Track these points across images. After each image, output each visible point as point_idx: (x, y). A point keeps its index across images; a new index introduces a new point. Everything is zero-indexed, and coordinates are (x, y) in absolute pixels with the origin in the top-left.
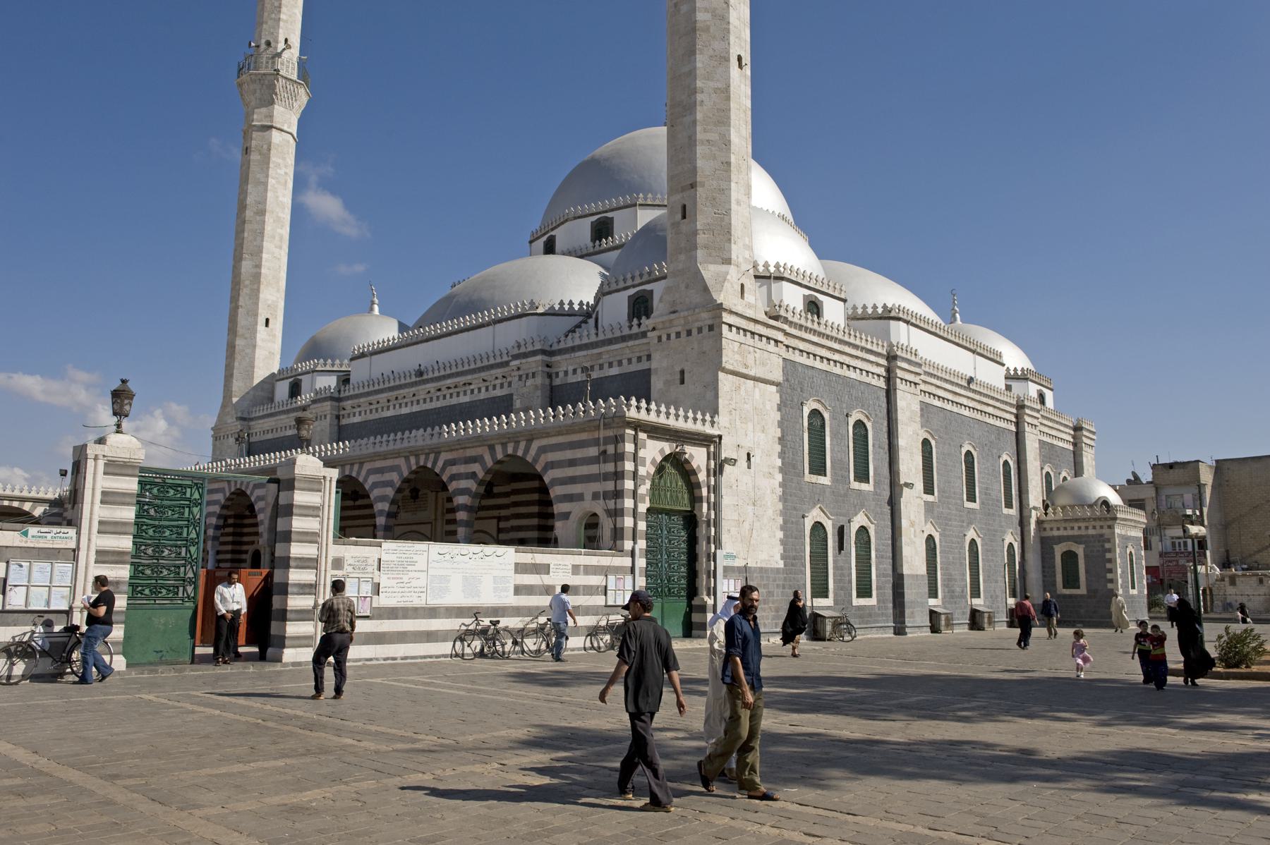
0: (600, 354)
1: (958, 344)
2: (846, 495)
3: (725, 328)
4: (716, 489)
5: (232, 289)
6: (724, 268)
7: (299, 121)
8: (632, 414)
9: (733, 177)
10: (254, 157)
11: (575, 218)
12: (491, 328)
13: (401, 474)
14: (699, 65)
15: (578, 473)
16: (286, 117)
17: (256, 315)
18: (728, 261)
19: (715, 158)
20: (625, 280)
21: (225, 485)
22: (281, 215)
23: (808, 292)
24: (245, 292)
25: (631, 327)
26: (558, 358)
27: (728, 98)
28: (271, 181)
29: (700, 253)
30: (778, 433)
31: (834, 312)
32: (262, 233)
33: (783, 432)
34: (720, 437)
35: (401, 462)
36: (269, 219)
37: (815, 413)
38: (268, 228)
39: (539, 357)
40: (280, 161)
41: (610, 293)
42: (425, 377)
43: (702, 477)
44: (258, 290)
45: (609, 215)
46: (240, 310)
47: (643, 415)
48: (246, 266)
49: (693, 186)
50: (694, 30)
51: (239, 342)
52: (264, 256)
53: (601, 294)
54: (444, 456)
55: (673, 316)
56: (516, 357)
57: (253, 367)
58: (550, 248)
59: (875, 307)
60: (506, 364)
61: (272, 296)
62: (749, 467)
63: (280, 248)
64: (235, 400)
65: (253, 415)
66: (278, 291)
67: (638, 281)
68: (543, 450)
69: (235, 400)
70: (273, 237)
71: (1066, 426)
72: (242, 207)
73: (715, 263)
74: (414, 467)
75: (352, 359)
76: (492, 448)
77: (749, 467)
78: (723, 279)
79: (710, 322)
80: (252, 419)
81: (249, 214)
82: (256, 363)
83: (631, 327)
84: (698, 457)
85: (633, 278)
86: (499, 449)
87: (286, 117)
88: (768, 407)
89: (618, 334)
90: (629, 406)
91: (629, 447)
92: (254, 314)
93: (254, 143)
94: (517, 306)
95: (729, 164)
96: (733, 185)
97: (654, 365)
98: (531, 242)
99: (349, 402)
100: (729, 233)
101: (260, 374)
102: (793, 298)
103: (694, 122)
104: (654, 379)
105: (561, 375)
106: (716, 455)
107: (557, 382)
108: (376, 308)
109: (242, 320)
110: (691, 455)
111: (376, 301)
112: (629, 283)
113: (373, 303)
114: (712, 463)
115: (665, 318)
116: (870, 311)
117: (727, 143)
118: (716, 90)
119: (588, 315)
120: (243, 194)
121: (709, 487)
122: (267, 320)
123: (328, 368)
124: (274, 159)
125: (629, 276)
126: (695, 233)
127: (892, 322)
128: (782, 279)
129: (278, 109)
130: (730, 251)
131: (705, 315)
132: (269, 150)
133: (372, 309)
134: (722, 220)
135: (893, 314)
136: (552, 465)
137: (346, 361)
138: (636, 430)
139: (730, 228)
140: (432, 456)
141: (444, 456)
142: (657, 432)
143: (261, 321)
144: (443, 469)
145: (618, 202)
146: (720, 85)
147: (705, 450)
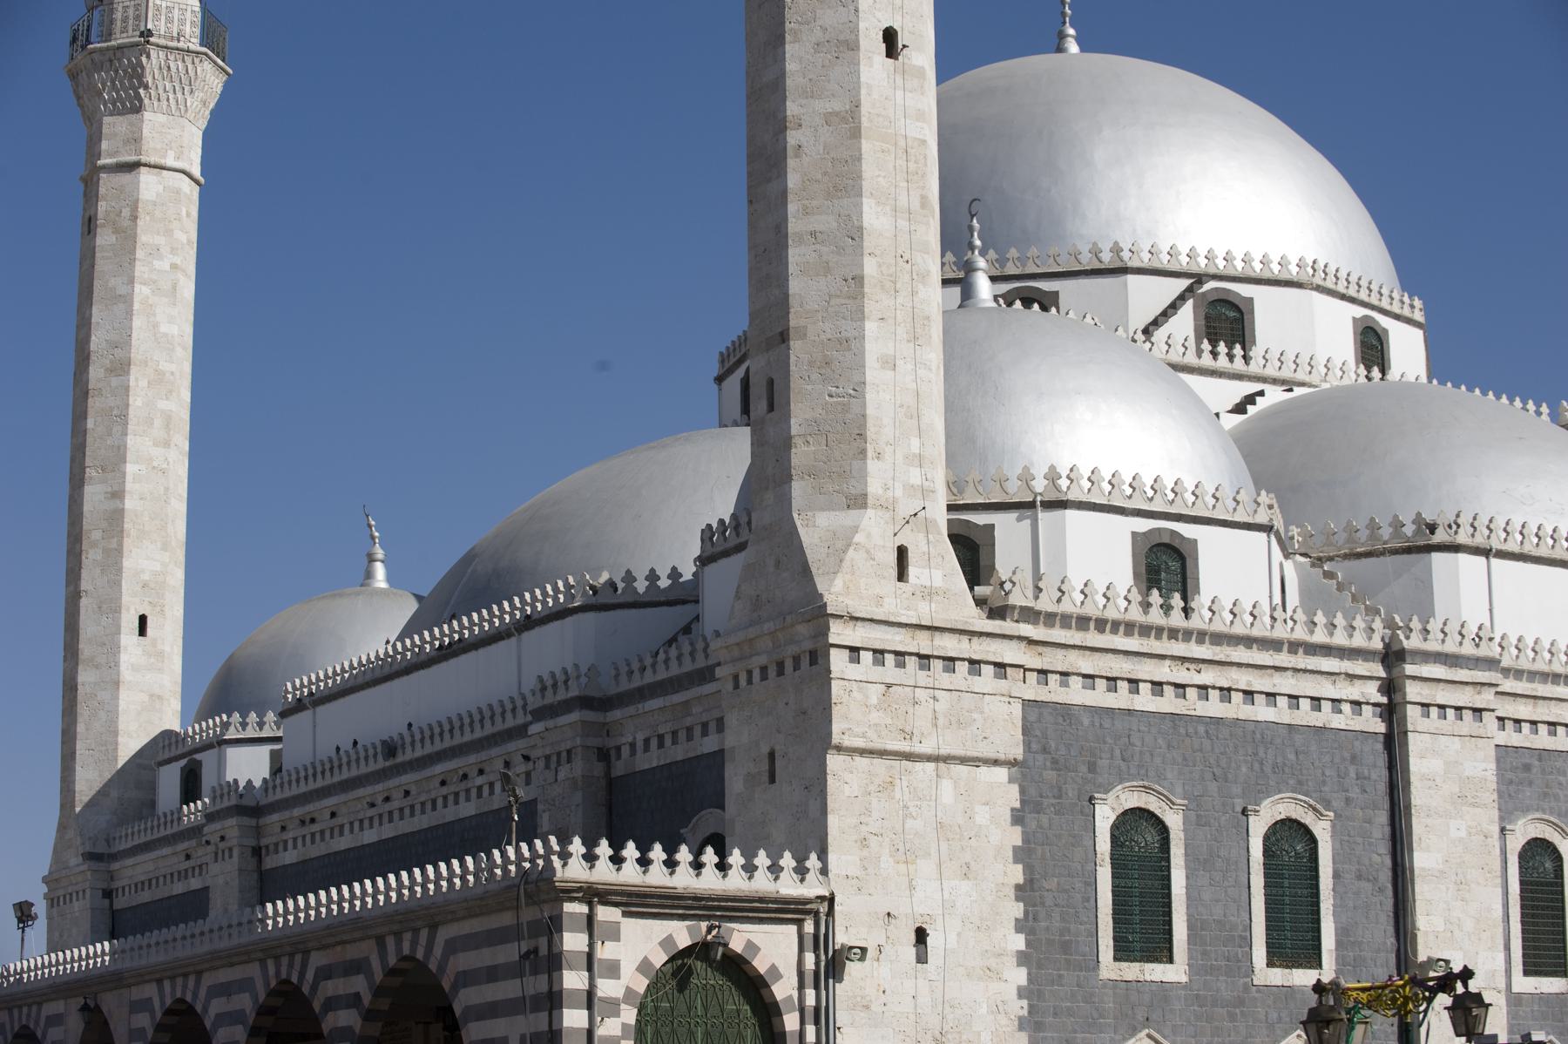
0: (686, 703)
2: (1241, 1002)
4: (821, 1016)
5: (69, 552)
6: (845, 518)
7: (206, 135)
8: (574, 870)
9: (870, 306)
10: (104, 238)
13: (255, 998)
14: (790, 66)
15: (500, 996)
16: (172, 131)
17: (117, 610)
18: (859, 501)
19: (827, 269)
21: (367, 949)
22: (165, 366)
23: (1144, 525)
24: (91, 557)
26: (617, 714)
27: (856, 133)
28: (141, 291)
29: (798, 489)
30: (1017, 874)
31: (1239, 573)
32: (123, 417)
33: (1029, 870)
34: (831, 900)
35: (253, 970)
36: (138, 380)
37: (1134, 821)
38: (137, 402)
39: (574, 716)
40: (160, 240)
42: (400, 759)
43: (784, 990)
44: (119, 551)
46: (84, 602)
47: (604, 872)
48: (94, 496)
49: (784, 337)
51: (85, 677)
52: (131, 468)
54: (317, 960)
56: (540, 714)
57: (116, 733)
60: (521, 731)
61: (151, 556)
62: (922, 959)
63: (167, 444)
64: (78, 809)
65: (114, 850)
66: (165, 547)
68: (452, 947)
69: (78, 809)
70: (150, 422)
71: (492, 1010)
72: (83, 358)
73: (830, 507)
74: (392, 960)
75: (283, 715)
76: (381, 941)
77: (922, 959)
78: (842, 543)
79: (808, 645)
80: (114, 857)
81: (95, 372)
82: (122, 725)
84: (774, 949)
86: (390, 942)
87: (172, 131)
88: (982, 816)
90: (565, 856)
91: (574, 941)
92: (112, 607)
93: (102, 207)
95: (859, 280)
96: (870, 327)
97: (730, 740)
98: (719, 380)
99: (275, 817)
100: (862, 435)
101: (130, 743)
104: (729, 771)
105: (625, 751)
106: (820, 942)
107: (619, 769)
108: (380, 571)
109: (89, 626)
110: (750, 945)
111: (379, 553)
113: (371, 559)
114: (810, 958)
116: (1386, 532)
117: (855, 234)
118: (829, 118)
120: (84, 326)
121: (802, 1010)
122: (143, 620)
123: (251, 733)
124: (146, 236)
127: (1436, 557)
128: (1062, 504)
129: (153, 120)
130: (863, 476)
131: (803, 629)
132: (134, 218)
133: (369, 574)
134: (846, 408)
135: (1440, 537)
136: (467, 978)
137: (271, 716)
138: (590, 904)
139: (863, 425)
140: (298, 958)
141: (317, 960)
142: (640, 903)
143: (130, 622)
144: (314, 987)
146: (836, 105)
147: (793, 928)
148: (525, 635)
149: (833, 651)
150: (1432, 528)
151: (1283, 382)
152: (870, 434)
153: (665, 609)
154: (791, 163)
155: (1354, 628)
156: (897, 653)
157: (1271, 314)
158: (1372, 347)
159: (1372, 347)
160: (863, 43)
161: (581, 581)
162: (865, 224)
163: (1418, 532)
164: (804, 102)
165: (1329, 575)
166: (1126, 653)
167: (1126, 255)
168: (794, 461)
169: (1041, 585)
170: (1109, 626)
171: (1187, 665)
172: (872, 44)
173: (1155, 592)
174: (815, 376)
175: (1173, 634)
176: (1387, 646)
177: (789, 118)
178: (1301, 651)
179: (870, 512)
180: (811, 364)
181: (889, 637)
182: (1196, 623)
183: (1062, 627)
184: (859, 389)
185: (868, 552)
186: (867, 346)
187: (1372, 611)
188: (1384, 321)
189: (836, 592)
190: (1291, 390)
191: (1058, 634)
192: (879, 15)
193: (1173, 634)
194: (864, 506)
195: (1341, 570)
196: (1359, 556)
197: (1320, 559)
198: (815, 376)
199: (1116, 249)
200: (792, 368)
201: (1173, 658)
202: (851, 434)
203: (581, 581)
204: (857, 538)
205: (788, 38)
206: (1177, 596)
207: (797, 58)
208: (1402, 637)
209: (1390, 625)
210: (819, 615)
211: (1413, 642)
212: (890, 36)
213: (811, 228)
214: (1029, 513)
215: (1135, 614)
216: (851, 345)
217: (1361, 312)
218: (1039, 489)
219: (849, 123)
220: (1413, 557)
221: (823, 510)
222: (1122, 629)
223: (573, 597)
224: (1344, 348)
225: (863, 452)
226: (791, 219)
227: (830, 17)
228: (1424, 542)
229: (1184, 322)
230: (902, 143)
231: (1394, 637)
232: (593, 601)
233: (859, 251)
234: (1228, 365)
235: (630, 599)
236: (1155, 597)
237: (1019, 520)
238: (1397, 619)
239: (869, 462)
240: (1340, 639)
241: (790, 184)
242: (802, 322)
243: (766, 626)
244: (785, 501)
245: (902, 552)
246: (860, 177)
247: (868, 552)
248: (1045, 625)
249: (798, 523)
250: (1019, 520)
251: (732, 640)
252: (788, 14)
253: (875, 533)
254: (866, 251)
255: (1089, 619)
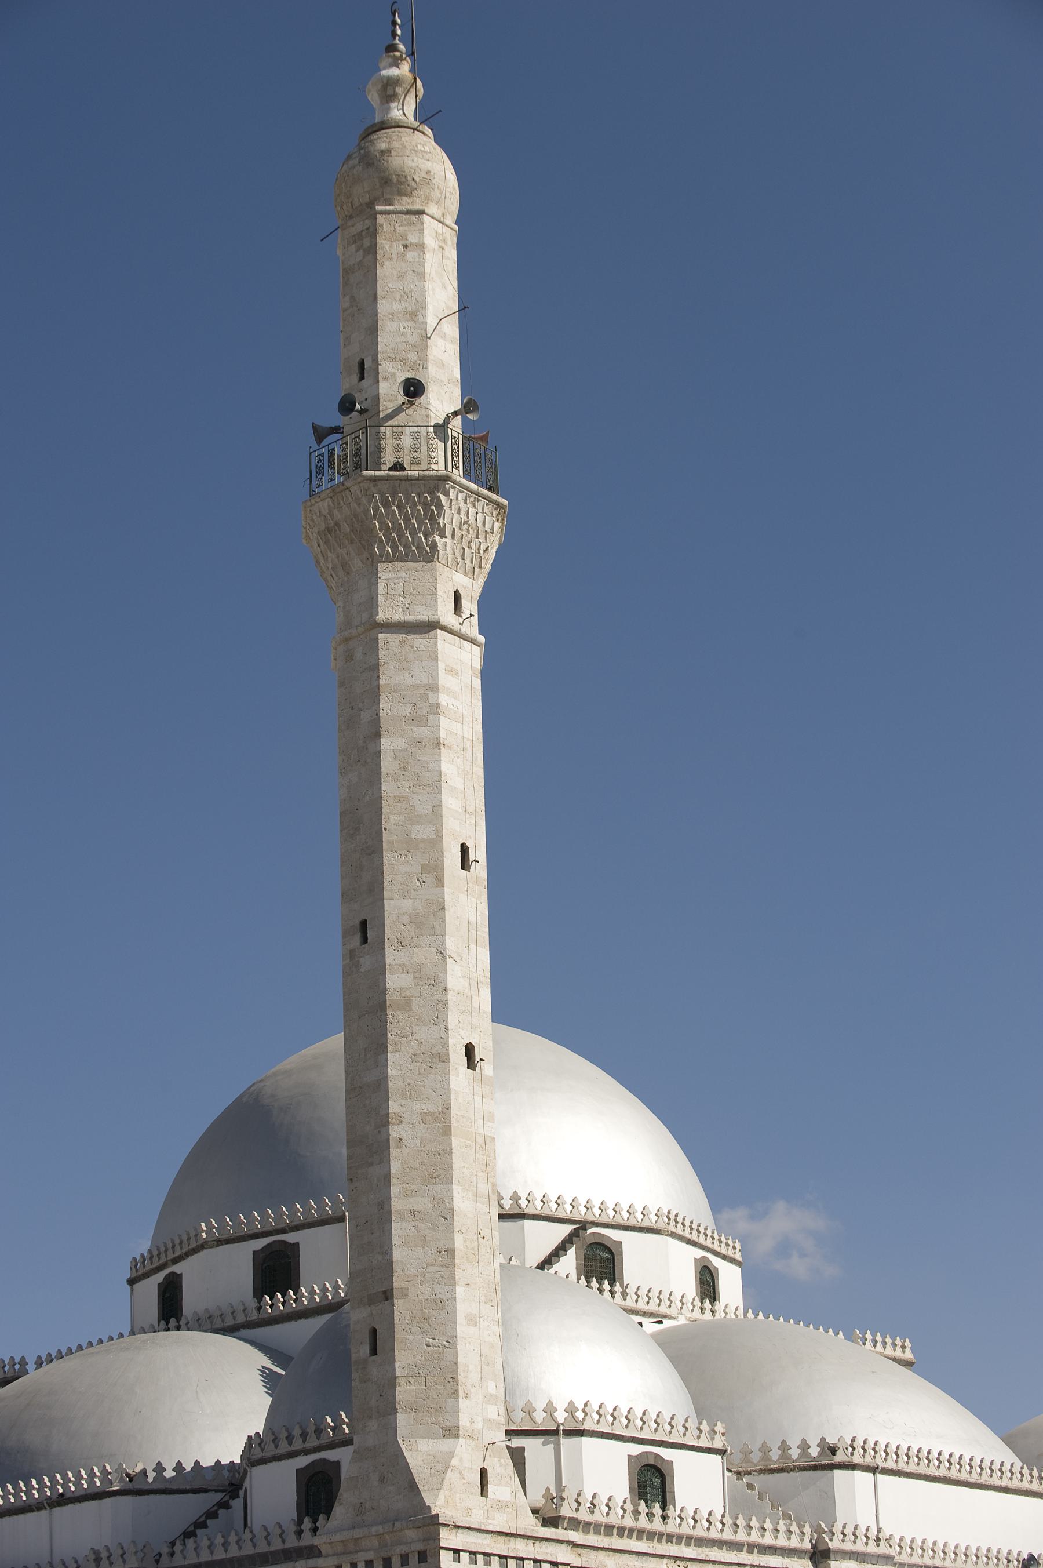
1: (1006, 1490)
3: (445, 1557)
6: (445, 1445)
9: (459, 1274)
11: (220, 1242)
12: (44, 1513)
14: (392, 1071)
18: (453, 1432)
19: (424, 1243)
20: (290, 1439)
23: (637, 1449)
25: (299, 1533)
27: (447, 1131)
29: (402, 1420)
31: (699, 1485)
41: (263, 1461)
45: (290, 1238)
49: (388, 1295)
50: (382, 1006)
53: (257, 1452)
55: (358, 1533)
58: (170, 1310)
59: (804, 1446)
67: (312, 1442)
73: (428, 1436)
78: (442, 1465)
79: (419, 1546)
83: (299, 1533)
85: (304, 1435)
89: (277, 1545)
94: (92, 1475)
95: (451, 1252)
96: (460, 1290)
98: (132, 1282)
100: (454, 1379)
102: (602, 1474)
103: (387, 1178)
112: (298, 1444)
115: (346, 1535)
116: (795, 1453)
117: (448, 1215)
118: (424, 1117)
119: (226, 1485)
125: (297, 1432)
126: (392, 1382)
127: (837, 1473)
128: (580, 1433)
130: (456, 1412)
131: (411, 1534)
134: (441, 1356)
139: (456, 1371)
145: (307, 1209)
146: (430, 1107)
148: (57, 1510)
149: (442, 1552)
150: (833, 1451)
151: (651, 1315)
152: (461, 1378)
153: (190, 1495)
154: (393, 1152)
155: (751, 1528)
156: (485, 1554)
157: (637, 1255)
158: (707, 1284)
159: (707, 1284)
160: (452, 1057)
161: (119, 1469)
162: (455, 1207)
163: (820, 1454)
164: (403, 1102)
165: (750, 1486)
166: (638, 1553)
167: (523, 1203)
168: (399, 1397)
169: (564, 1495)
170: (615, 1531)
171: (678, 1563)
172: (458, 1057)
173: (642, 1502)
174: (415, 1329)
175: (651, 1536)
176: (814, 1546)
177: (391, 1115)
178: (756, 1551)
179: (461, 1441)
180: (412, 1319)
181: (479, 1541)
182: (672, 1527)
183: (595, 1533)
184: (452, 1341)
185: (461, 1473)
186: (458, 1306)
187: (787, 1517)
188: (716, 1261)
189: (442, 1503)
190: (661, 1322)
191: (592, 1539)
192: (462, 1032)
193: (651, 1536)
194: (457, 1436)
195: (758, 1481)
196: (772, 1471)
197: (738, 1473)
198: (415, 1329)
199: (515, 1198)
200: (396, 1321)
201: (670, 1557)
202: (449, 1378)
203: (119, 1469)
204: (454, 1462)
205: (390, 1047)
206: (657, 1505)
207: (398, 1065)
208: (827, 1540)
209: (818, 1530)
210: (432, 1523)
211: (834, 1544)
212: (469, 1050)
213: (410, 1207)
214: (552, 1439)
215: (629, 1522)
216: (444, 1304)
217: (700, 1253)
218: (561, 1420)
219: (441, 1122)
220: (819, 1473)
221: (422, 1437)
222: (635, 1534)
223: (111, 1483)
224: (688, 1285)
225: (456, 1392)
226: (393, 1199)
227: (425, 1033)
228: (828, 1461)
229: (569, 1262)
230: (480, 1140)
231: (820, 1537)
232: (130, 1486)
233: (450, 1229)
234: (623, 1303)
235: (161, 1486)
236: (642, 1507)
237: (544, 1444)
238: (823, 1525)
239: (460, 1400)
240: (782, 1541)
241: (393, 1170)
242: (404, 1284)
243: (374, 1529)
244: (392, 1430)
245: (483, 1473)
246: (451, 1168)
247: (461, 1473)
248: (583, 1531)
249: (403, 1448)
250: (544, 1444)
251: (338, 1537)
252: (390, 1028)
253: (466, 1458)
254: (456, 1230)
255: (614, 1527)
